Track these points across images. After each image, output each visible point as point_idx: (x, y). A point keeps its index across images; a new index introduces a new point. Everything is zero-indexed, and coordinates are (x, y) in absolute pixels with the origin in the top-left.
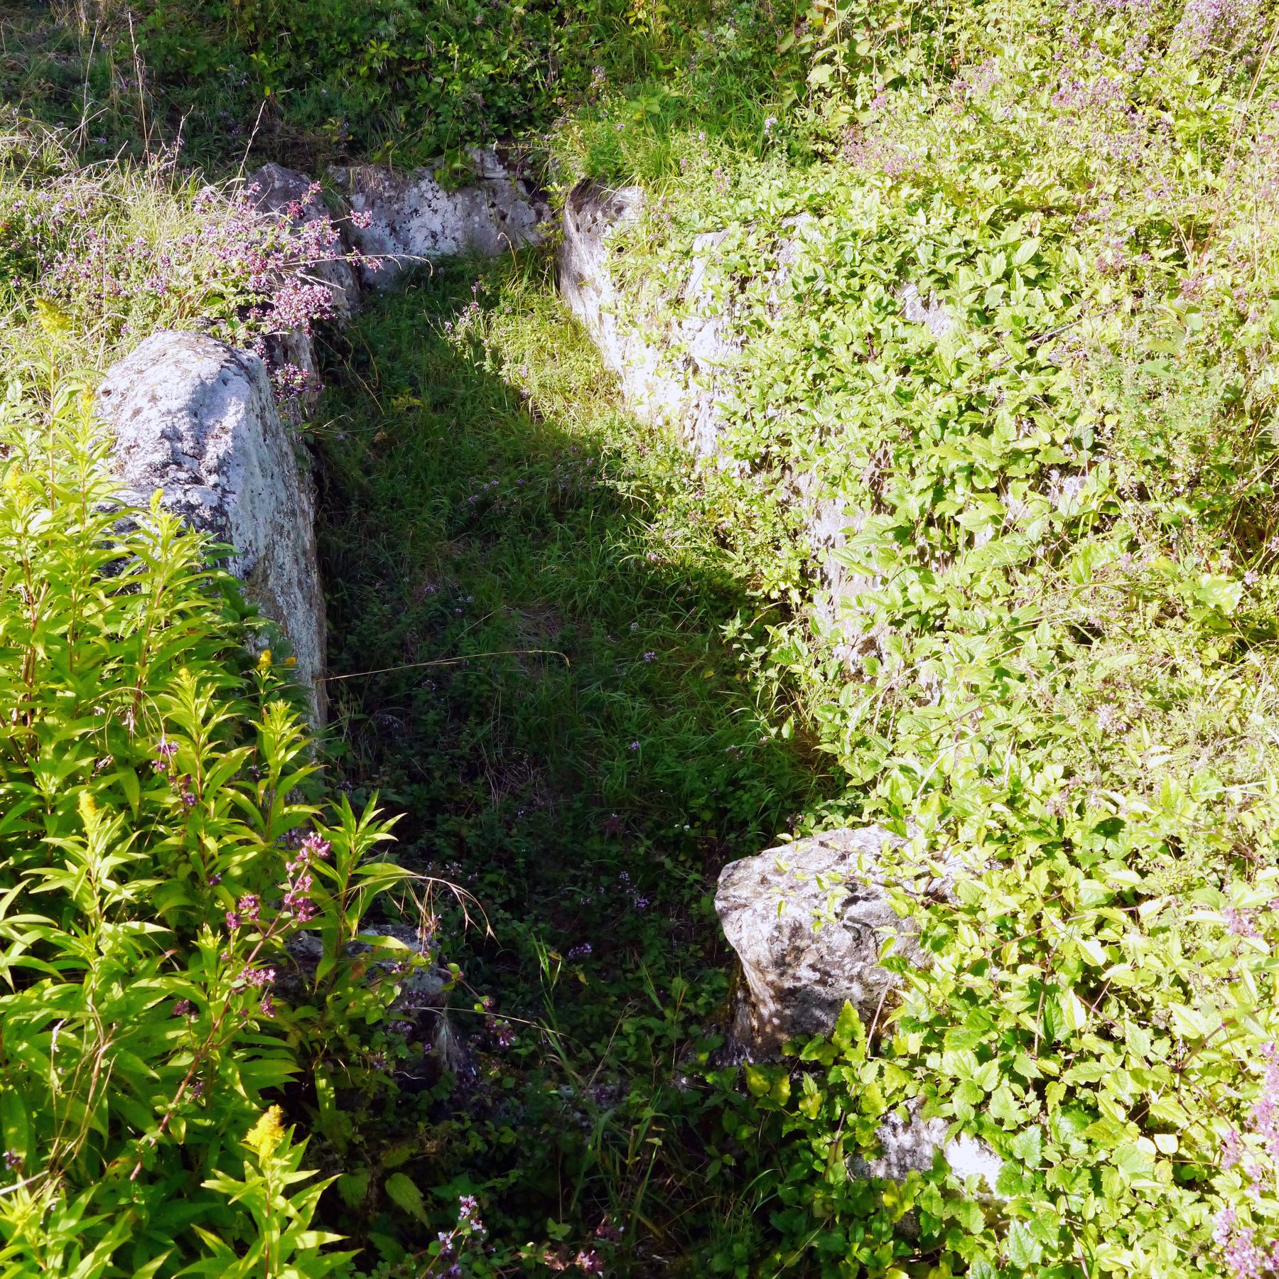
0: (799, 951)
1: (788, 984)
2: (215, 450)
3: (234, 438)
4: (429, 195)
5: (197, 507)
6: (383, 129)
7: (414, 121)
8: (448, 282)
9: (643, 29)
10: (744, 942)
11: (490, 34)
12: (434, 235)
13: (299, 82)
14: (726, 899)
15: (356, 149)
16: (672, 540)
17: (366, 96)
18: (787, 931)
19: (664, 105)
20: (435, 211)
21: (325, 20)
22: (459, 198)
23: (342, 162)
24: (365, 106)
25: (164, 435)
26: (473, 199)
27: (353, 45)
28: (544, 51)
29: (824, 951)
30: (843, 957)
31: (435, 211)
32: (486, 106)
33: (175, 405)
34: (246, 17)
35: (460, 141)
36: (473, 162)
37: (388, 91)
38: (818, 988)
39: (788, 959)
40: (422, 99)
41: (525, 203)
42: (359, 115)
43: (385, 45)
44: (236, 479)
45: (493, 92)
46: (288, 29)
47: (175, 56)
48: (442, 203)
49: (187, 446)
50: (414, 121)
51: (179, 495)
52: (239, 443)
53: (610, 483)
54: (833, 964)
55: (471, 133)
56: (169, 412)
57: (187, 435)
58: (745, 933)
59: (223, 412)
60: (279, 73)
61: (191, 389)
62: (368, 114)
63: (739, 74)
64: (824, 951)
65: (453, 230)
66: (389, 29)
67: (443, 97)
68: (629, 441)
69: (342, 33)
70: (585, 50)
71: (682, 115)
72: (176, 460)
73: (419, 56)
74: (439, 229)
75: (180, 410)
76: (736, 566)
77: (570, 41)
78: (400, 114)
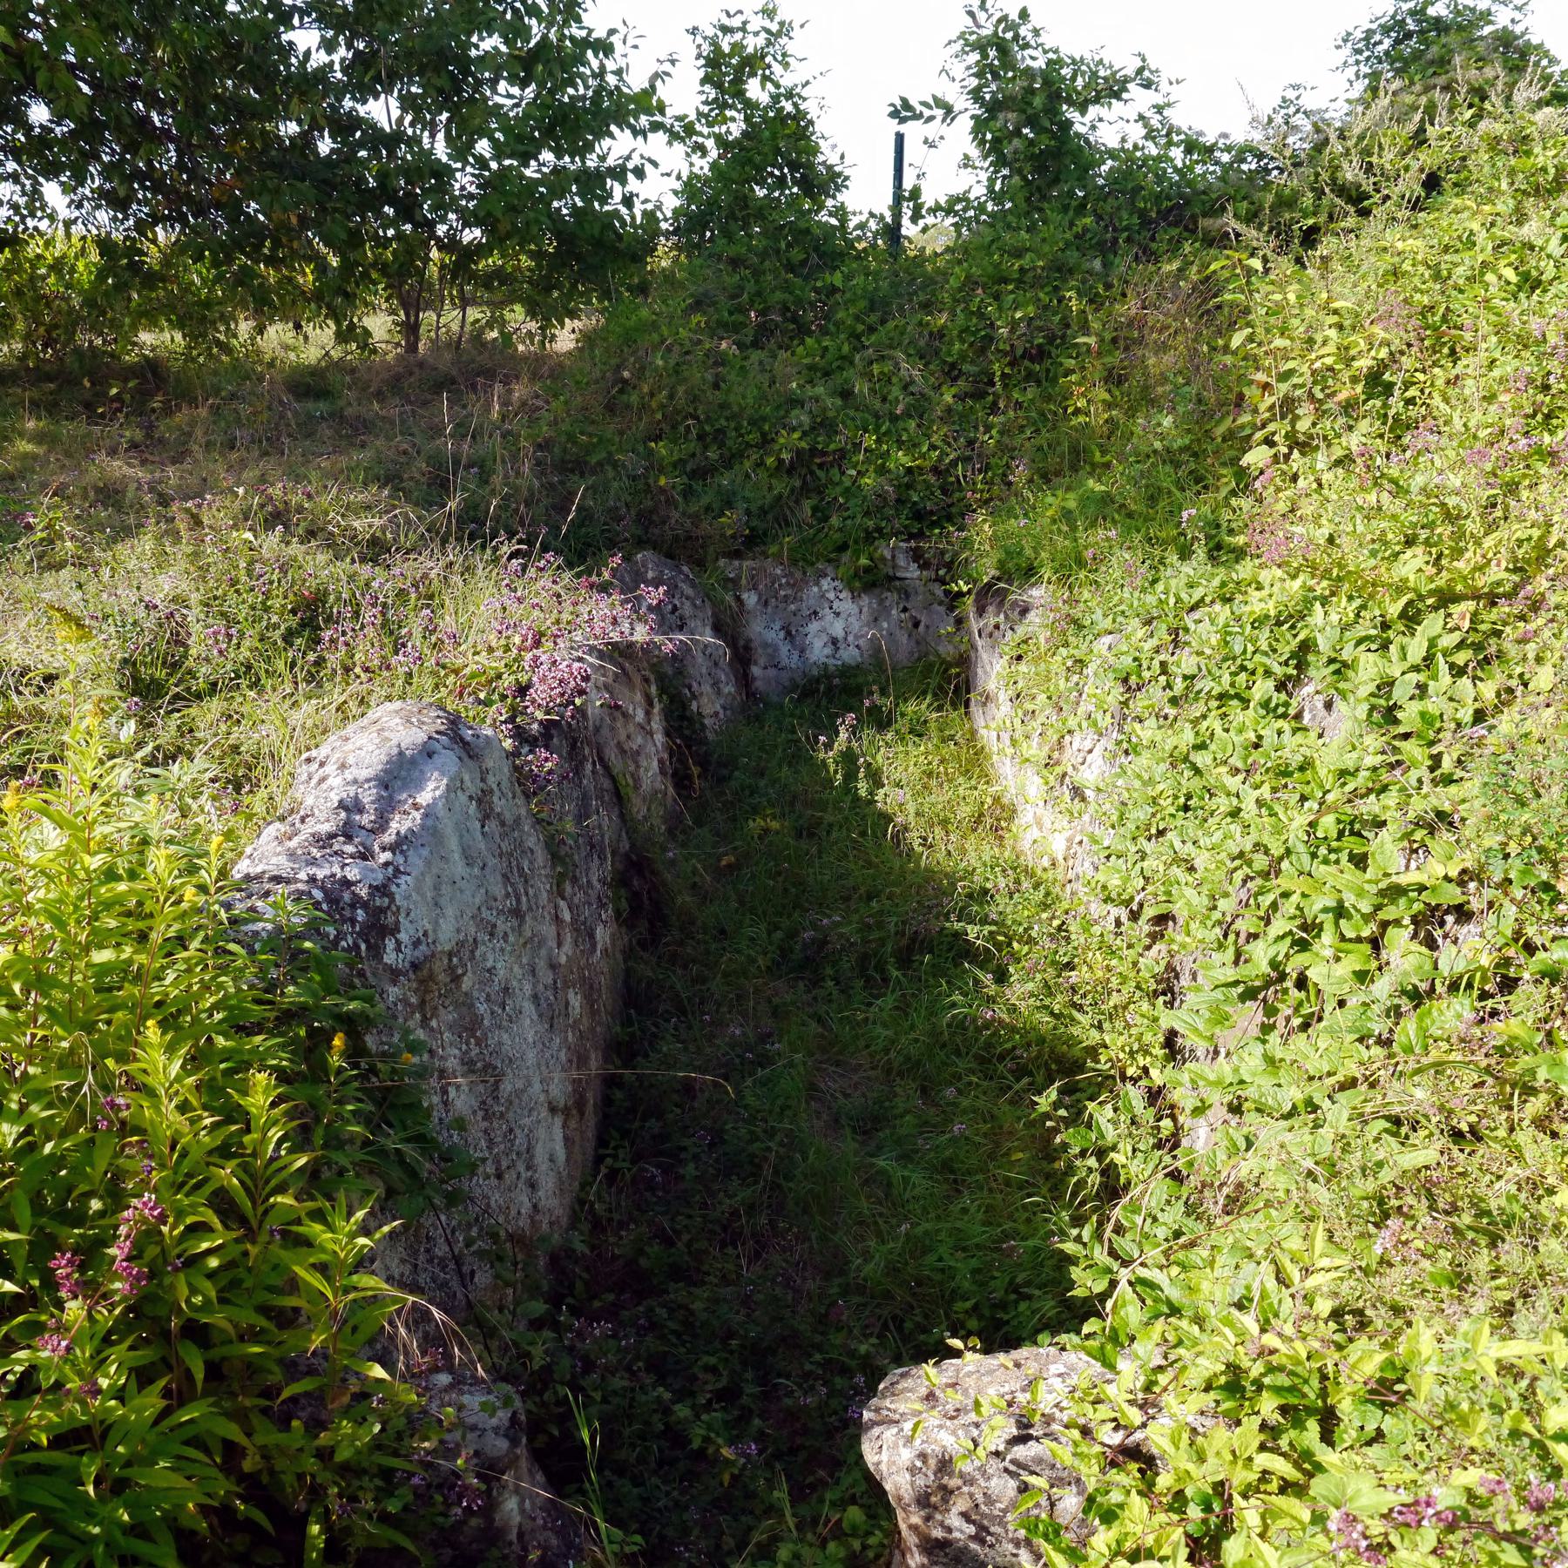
0: (947, 1492)
1: (938, 1533)
2: (399, 824)
3: (426, 816)
4: (831, 595)
5: (354, 883)
6: (787, 524)
7: (821, 514)
8: (838, 692)
9: (1081, 419)
10: (883, 1467)
11: (912, 424)
12: (834, 641)
13: (702, 473)
14: (877, 1410)
15: (752, 542)
16: (1021, 996)
17: (770, 489)
18: (932, 1462)
19: (1084, 501)
20: (838, 614)
21: (736, 409)
22: (865, 600)
23: (737, 555)
24: (769, 499)
25: (342, 805)
26: (881, 602)
27: (764, 435)
28: (971, 443)
29: (980, 1498)
30: (1005, 1511)
31: (838, 614)
32: (898, 501)
33: (364, 774)
34: (654, 404)
35: (869, 537)
36: (883, 559)
37: (798, 483)
38: (974, 1546)
39: (933, 1499)
40: (832, 492)
41: (942, 609)
42: (761, 508)
43: (796, 435)
44: (416, 860)
45: (909, 486)
46: (696, 418)
47: (575, 443)
48: (846, 605)
49: (366, 819)
50: (821, 514)
51: (336, 869)
52: (430, 822)
53: (958, 926)
54: (992, 1518)
55: (879, 530)
56: (355, 781)
57: (370, 808)
58: (884, 1457)
59: (420, 787)
60: (681, 462)
61: (384, 758)
62: (772, 507)
63: (1177, 465)
64: (980, 1498)
65: (857, 637)
66: (801, 417)
67: (853, 490)
68: (1002, 883)
69: (752, 422)
70: (1017, 442)
71: (1103, 509)
72: (347, 832)
73: (832, 447)
74: (840, 633)
75: (368, 780)
76: (1084, 1030)
77: (1001, 433)
78: (807, 506)
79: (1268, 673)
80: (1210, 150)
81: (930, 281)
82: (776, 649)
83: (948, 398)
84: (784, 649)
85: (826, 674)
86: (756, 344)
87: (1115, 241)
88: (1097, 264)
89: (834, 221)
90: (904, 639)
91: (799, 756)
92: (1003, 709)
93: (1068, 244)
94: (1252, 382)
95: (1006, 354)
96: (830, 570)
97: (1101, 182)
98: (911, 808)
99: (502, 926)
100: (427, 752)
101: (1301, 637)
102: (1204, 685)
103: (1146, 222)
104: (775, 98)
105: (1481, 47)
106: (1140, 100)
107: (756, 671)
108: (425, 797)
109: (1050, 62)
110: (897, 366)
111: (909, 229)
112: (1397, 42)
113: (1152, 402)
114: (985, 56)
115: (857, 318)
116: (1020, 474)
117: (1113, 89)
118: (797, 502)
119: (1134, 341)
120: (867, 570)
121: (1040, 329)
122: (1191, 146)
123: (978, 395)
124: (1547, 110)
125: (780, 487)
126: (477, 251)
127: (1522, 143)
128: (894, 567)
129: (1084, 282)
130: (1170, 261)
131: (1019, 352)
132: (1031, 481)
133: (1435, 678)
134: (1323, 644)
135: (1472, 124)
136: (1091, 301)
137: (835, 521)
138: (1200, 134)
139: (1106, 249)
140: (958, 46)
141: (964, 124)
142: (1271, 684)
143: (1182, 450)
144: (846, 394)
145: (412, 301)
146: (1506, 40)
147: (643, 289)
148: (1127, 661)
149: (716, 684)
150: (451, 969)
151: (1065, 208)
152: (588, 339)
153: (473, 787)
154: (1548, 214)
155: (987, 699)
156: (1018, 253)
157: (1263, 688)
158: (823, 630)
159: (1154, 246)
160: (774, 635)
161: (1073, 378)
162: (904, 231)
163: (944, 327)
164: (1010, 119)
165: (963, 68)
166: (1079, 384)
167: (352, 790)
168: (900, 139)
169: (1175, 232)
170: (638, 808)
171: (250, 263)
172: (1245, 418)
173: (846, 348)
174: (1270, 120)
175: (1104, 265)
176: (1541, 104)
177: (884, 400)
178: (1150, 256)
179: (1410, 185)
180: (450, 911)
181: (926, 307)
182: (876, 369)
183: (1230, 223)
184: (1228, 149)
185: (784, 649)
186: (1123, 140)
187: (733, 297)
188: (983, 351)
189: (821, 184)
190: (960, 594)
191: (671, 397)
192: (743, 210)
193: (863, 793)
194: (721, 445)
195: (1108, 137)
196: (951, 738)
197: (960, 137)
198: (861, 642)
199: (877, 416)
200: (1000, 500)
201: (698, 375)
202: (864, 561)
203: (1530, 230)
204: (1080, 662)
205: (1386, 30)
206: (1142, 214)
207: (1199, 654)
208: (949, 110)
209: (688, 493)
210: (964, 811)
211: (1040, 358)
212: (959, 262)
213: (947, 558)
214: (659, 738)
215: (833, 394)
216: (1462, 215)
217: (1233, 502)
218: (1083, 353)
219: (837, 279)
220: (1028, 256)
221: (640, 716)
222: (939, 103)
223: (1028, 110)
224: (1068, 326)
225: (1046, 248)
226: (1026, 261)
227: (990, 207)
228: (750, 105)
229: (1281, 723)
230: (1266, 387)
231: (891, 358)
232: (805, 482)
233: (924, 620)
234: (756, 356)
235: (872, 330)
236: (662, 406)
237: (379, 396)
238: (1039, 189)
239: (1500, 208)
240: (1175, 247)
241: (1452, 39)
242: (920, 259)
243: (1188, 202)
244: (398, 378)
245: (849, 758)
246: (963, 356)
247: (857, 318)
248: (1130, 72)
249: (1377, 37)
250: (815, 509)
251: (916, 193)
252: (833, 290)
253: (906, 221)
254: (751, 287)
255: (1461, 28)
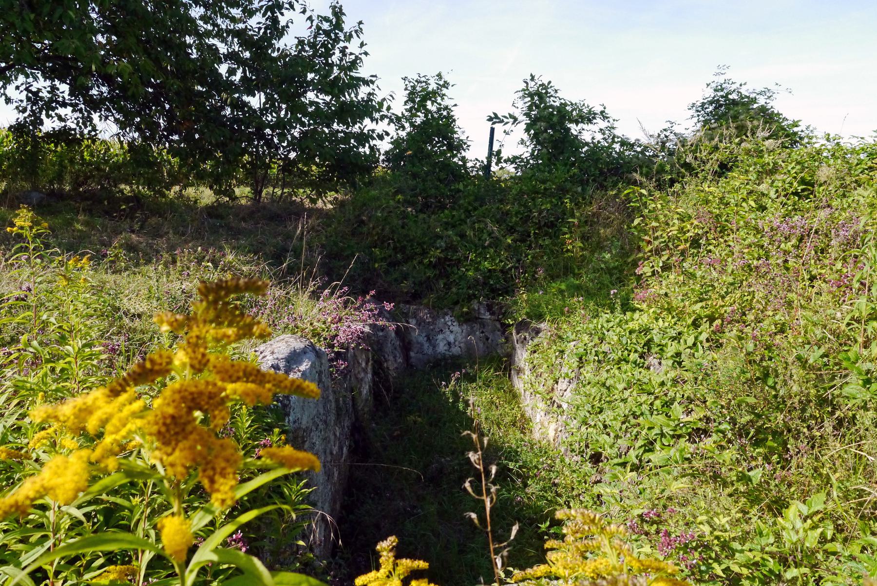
4: (450, 323)
7: (448, 286)
9: (570, 254)
12: (449, 344)
13: (394, 264)
17: (425, 273)
19: (569, 287)
20: (452, 332)
22: (465, 327)
23: (408, 302)
24: (424, 278)
26: (472, 328)
27: (423, 250)
31: (452, 332)
33: (281, 356)
34: (374, 233)
35: (470, 298)
36: (474, 309)
37: (438, 272)
41: (499, 333)
45: (489, 277)
46: (393, 239)
48: (456, 328)
50: (448, 286)
53: (505, 462)
59: (300, 363)
63: (611, 275)
65: (460, 343)
67: (463, 277)
69: (419, 244)
71: (578, 290)
73: (455, 257)
74: (452, 341)
79: (636, 351)
80: (632, 145)
81: (502, 190)
82: (422, 345)
83: (509, 241)
84: (426, 345)
85: (444, 358)
86: (421, 211)
87: (588, 181)
88: (579, 189)
89: (460, 163)
90: (481, 345)
91: (434, 390)
92: (527, 375)
93: (566, 180)
94: (643, 240)
95: (536, 224)
96: (450, 312)
97: (583, 155)
98: (483, 416)
99: (321, 427)
100: (304, 351)
101: (648, 337)
102: (613, 356)
103: (602, 173)
104: (439, 110)
105: (752, 112)
106: (601, 124)
107: (412, 354)
108: (303, 368)
109: (561, 104)
110: (486, 224)
111: (494, 168)
112: (716, 108)
113: (602, 248)
114: (533, 99)
115: (469, 203)
116: (541, 273)
117: (588, 117)
118: (437, 280)
119: (595, 223)
120: (467, 313)
121: (553, 215)
122: (623, 143)
123: (523, 241)
124: (770, 141)
125: (429, 273)
126: (294, 162)
127: (759, 153)
128: (479, 313)
129: (573, 196)
130: (612, 190)
131: (543, 223)
132: (545, 278)
133: (697, 351)
134: (656, 340)
135: (739, 144)
136: (576, 204)
137: (454, 290)
138: (628, 139)
139: (584, 183)
140: (521, 94)
141: (523, 126)
142: (637, 355)
143: (615, 268)
144: (463, 236)
145: (258, 180)
146: (763, 110)
147: (370, 183)
148: (581, 350)
149: (395, 357)
150: (303, 437)
151: (566, 165)
152: (340, 205)
153: (318, 369)
154: (770, 181)
155: (519, 371)
156: (544, 182)
157: (633, 356)
158: (445, 339)
159: (605, 184)
160: (422, 339)
161: (567, 236)
162: (492, 169)
163: (509, 210)
164: (542, 125)
165: (523, 105)
166: (569, 239)
167: (276, 361)
168: (492, 131)
169: (615, 178)
170: (360, 405)
171: (192, 158)
172: (641, 255)
173: (463, 217)
174: (659, 135)
175: (582, 190)
176: (768, 139)
177: (480, 240)
178: (603, 187)
179: (712, 166)
180: (306, 413)
181: (501, 201)
182: (476, 225)
183: (637, 176)
184: (640, 146)
185: (426, 345)
186: (593, 138)
187: (412, 190)
188: (526, 222)
189: (457, 146)
190: (509, 325)
191: (383, 230)
192: (421, 155)
193: (461, 408)
194: (404, 253)
195: (586, 137)
196: (502, 388)
197: (519, 132)
198: (462, 345)
199: (476, 246)
200: (531, 285)
201: (396, 222)
202: (465, 310)
203: (763, 188)
204: (562, 352)
205: (711, 103)
206: (601, 170)
207: (609, 343)
208: (515, 119)
209: (387, 272)
210: (508, 419)
211: (552, 227)
212: (517, 184)
213: (503, 311)
214: (370, 376)
215: (456, 235)
216: (736, 179)
217: (636, 290)
218: (571, 226)
219: (461, 186)
220: (548, 183)
221: (364, 365)
222: (511, 116)
223: (550, 121)
224: (565, 214)
225: (557, 181)
226: (548, 185)
227: (531, 162)
228: (427, 112)
229: (641, 369)
230: (649, 242)
231: (483, 221)
232: (441, 272)
233: (491, 337)
234: (421, 216)
235: (475, 209)
236: (377, 234)
237: (244, 219)
238: (554, 156)
239: (750, 177)
240: (615, 185)
241: (740, 109)
242: (499, 180)
243: (621, 166)
244: (253, 212)
245: (455, 394)
246: (516, 223)
247: (469, 203)
248: (598, 112)
249: (707, 106)
250: (445, 284)
251: (499, 152)
252: (459, 191)
253: (493, 164)
254: (421, 186)
255: (743, 104)
